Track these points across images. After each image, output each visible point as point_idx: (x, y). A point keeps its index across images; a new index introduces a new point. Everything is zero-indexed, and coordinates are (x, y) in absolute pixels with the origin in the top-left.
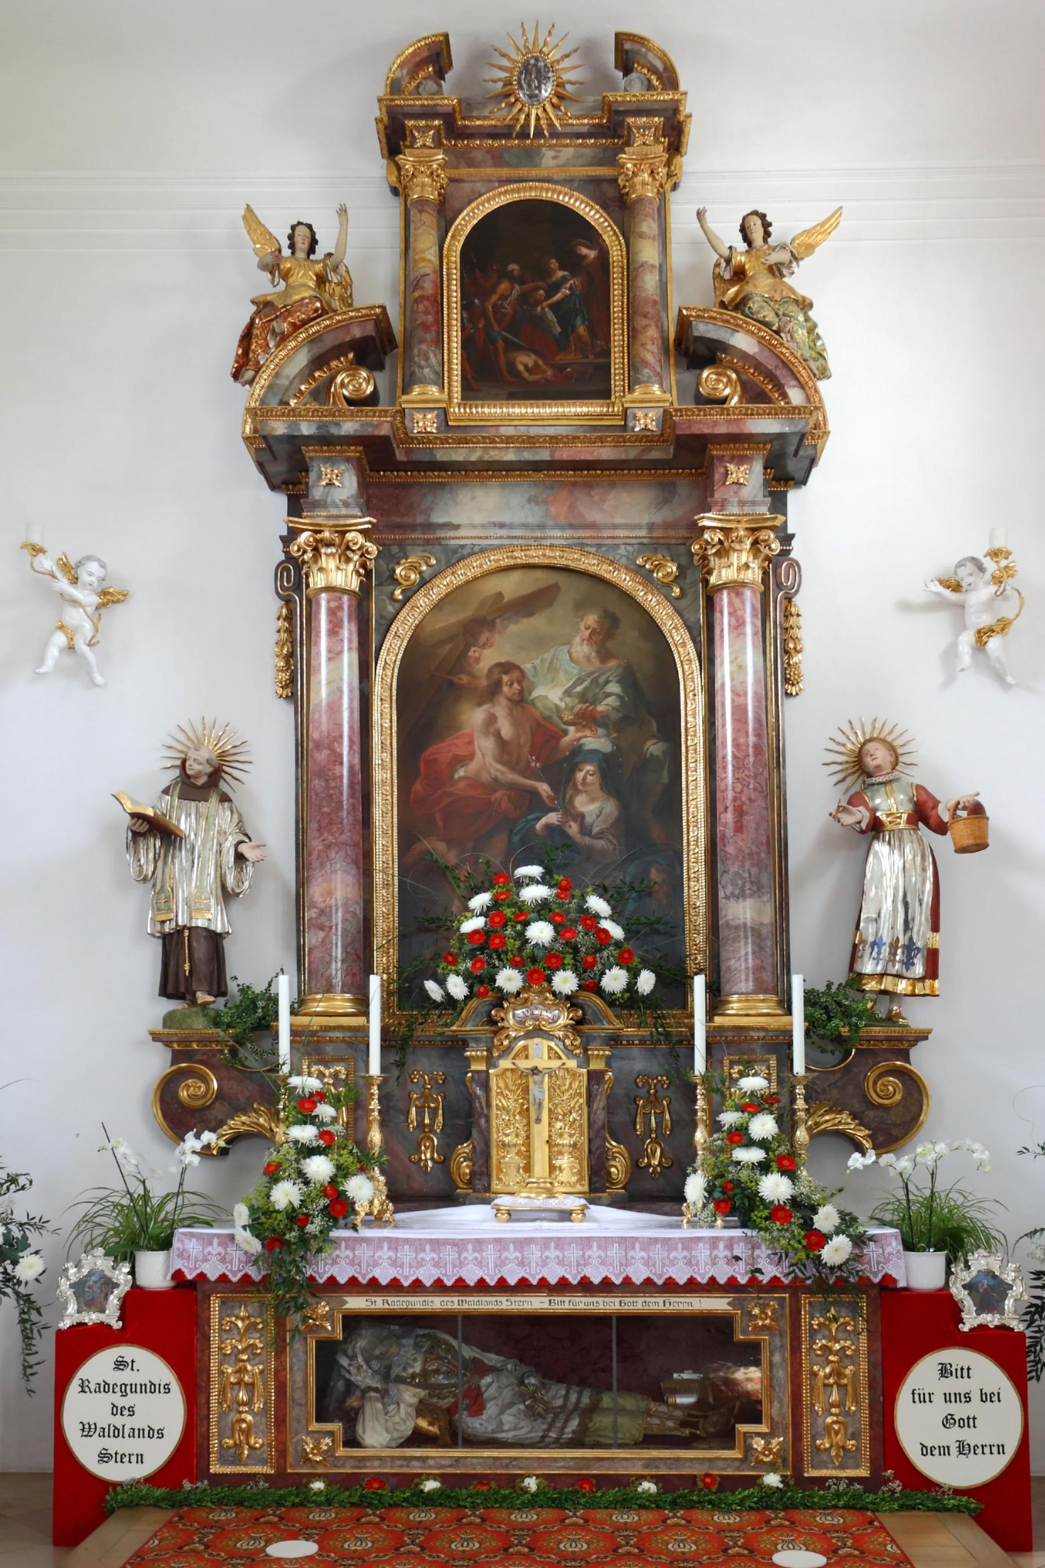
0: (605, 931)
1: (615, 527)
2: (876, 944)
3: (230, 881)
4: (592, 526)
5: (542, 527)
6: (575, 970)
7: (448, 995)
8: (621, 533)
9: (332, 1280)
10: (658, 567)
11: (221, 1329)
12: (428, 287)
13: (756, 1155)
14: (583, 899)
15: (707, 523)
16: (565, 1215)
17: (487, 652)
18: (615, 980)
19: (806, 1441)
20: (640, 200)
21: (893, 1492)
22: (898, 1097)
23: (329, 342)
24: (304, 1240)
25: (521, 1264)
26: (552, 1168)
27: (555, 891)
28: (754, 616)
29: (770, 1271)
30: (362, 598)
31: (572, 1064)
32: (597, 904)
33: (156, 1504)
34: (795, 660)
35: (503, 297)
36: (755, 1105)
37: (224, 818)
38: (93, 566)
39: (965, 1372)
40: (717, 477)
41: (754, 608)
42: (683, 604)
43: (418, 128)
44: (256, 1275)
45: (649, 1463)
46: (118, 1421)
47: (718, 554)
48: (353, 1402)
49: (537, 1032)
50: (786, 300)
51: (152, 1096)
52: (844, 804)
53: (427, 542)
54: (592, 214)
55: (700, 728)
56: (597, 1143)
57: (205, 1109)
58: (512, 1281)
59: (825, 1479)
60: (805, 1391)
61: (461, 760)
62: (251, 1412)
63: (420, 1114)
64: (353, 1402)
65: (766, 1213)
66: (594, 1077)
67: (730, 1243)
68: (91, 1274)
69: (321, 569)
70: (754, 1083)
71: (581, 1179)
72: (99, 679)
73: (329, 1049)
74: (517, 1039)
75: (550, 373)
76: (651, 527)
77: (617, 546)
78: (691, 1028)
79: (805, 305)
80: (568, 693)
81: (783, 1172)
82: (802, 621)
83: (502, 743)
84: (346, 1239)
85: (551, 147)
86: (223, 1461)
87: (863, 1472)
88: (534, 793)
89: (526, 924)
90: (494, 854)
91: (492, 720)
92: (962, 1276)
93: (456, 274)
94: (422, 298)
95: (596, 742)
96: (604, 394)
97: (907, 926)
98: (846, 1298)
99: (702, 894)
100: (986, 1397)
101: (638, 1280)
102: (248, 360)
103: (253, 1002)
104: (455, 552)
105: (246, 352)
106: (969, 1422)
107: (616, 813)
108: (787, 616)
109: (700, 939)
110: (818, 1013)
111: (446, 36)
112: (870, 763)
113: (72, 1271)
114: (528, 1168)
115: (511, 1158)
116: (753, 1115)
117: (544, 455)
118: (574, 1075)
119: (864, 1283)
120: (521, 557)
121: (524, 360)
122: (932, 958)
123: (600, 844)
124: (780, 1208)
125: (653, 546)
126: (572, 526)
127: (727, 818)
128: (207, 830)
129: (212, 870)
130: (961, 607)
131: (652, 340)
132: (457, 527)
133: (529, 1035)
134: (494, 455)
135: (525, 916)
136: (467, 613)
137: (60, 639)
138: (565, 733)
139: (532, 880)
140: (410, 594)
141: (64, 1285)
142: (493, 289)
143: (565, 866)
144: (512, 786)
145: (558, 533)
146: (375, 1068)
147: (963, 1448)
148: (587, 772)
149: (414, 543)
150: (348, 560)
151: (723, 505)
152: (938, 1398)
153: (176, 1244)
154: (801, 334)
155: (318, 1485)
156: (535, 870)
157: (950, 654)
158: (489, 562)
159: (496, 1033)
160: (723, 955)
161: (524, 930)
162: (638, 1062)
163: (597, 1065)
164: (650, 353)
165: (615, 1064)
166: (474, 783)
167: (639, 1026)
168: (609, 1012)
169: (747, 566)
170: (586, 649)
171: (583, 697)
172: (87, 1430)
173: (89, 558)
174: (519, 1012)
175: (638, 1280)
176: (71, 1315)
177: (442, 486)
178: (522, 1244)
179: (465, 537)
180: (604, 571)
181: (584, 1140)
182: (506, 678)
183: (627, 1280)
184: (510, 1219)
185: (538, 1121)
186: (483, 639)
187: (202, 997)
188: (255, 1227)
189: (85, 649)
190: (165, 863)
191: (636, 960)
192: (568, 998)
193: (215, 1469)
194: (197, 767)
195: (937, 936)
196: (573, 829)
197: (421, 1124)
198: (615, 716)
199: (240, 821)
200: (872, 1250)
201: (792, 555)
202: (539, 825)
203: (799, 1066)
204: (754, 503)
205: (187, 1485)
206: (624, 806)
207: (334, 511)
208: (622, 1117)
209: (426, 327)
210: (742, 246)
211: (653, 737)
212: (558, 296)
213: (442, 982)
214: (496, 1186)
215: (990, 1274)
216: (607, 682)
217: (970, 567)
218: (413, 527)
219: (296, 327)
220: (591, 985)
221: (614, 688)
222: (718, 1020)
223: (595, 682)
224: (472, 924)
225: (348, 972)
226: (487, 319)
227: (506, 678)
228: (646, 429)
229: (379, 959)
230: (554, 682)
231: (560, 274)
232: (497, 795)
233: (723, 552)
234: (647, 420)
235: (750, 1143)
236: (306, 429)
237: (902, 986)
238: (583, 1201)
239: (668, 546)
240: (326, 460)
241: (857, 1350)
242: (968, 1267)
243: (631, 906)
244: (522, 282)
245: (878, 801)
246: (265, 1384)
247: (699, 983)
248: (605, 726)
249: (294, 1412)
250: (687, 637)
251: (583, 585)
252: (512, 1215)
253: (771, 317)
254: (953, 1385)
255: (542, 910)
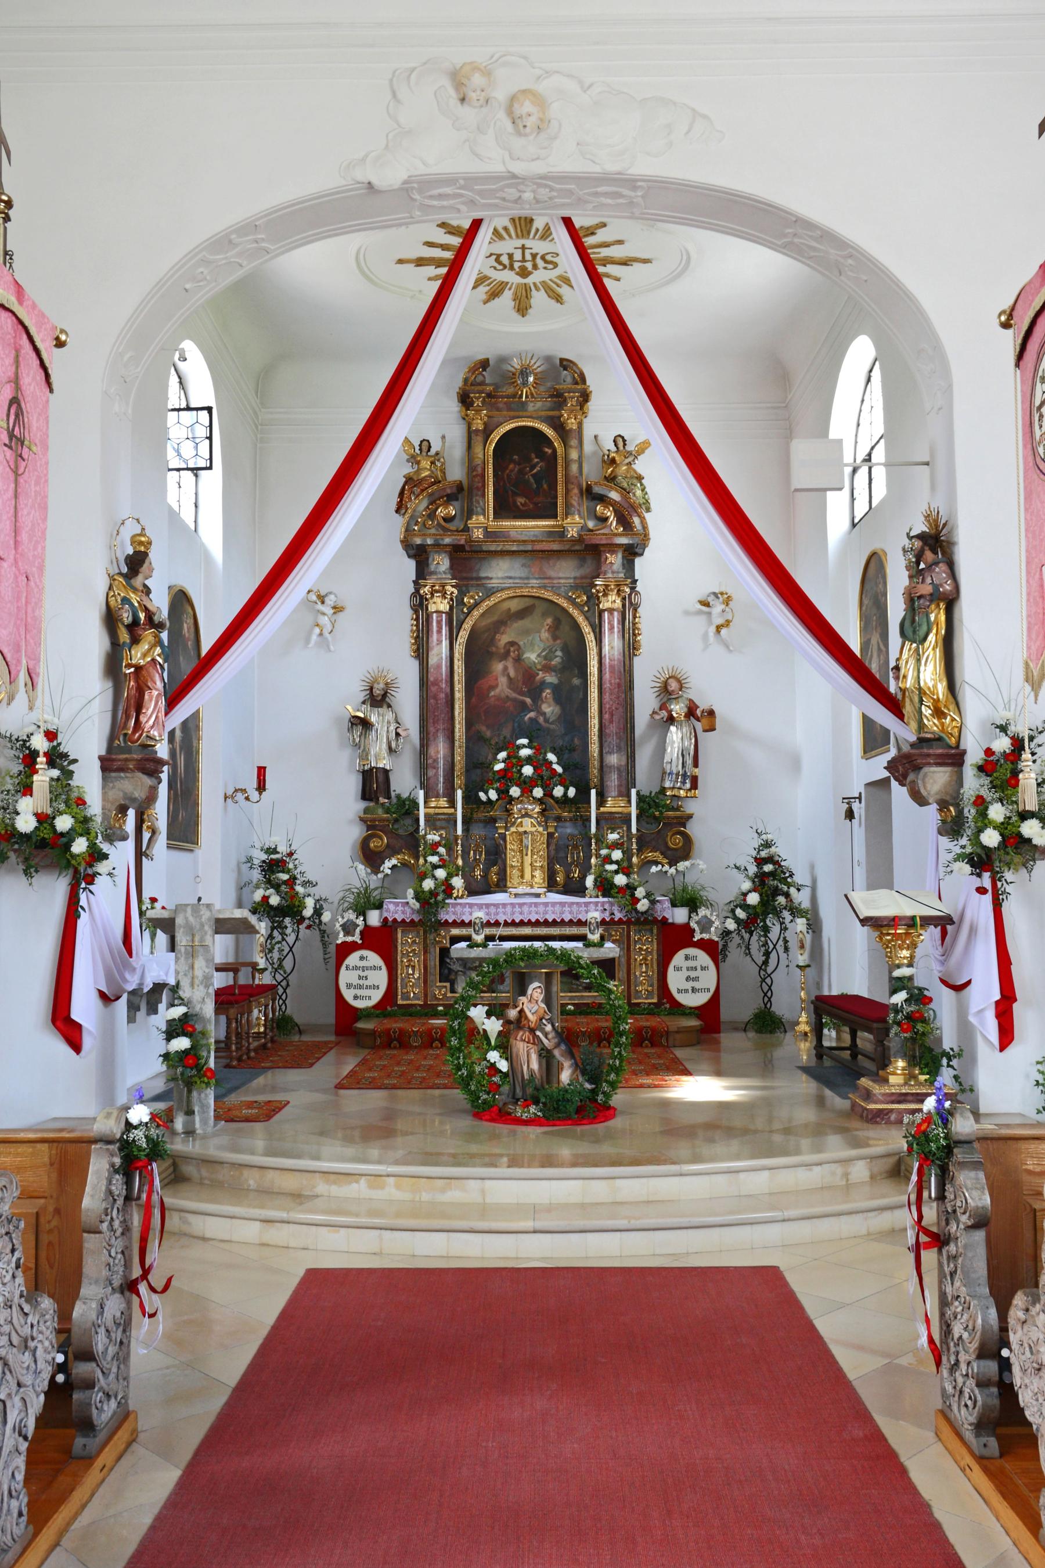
0: (555, 770)
1: (560, 578)
2: (671, 773)
3: (393, 745)
4: (549, 578)
5: (528, 578)
6: (542, 787)
7: (489, 799)
8: (562, 581)
9: (446, 920)
10: (579, 597)
11: (402, 943)
12: (479, 470)
13: (614, 867)
14: (545, 754)
15: (597, 583)
16: (538, 895)
17: (504, 636)
18: (558, 792)
19: (632, 988)
20: (571, 430)
21: (666, 1008)
22: (681, 844)
23: (437, 496)
24: (436, 902)
25: (521, 913)
26: (533, 876)
27: (533, 751)
28: (618, 623)
29: (618, 916)
30: (449, 614)
31: (541, 829)
32: (551, 757)
33: (377, 1016)
34: (638, 638)
35: (511, 471)
36: (614, 846)
37: (389, 716)
38: (332, 597)
39: (695, 958)
40: (603, 560)
41: (618, 620)
42: (588, 614)
43: (475, 397)
44: (416, 919)
45: (571, 998)
46: (361, 982)
47: (604, 595)
48: (452, 977)
49: (527, 815)
50: (632, 477)
51: (358, 847)
52: (657, 710)
53: (478, 585)
54: (549, 432)
55: (596, 673)
56: (551, 865)
57: (381, 852)
58: (517, 921)
59: (640, 1003)
60: (632, 966)
61: (493, 687)
62: (414, 978)
63: (475, 854)
64: (452, 977)
65: (616, 890)
66: (550, 835)
67: (603, 904)
68: (348, 921)
69: (434, 603)
70: (613, 837)
71: (544, 882)
72: (332, 647)
73: (438, 823)
74: (518, 818)
75: (531, 506)
76: (575, 578)
77: (560, 587)
78: (463, 808)
79: (640, 478)
80: (539, 656)
81: (624, 874)
82: (641, 620)
83: (510, 678)
84: (452, 904)
85: (532, 402)
86: (402, 999)
87: (655, 1001)
88: (524, 703)
89: (522, 766)
90: (506, 732)
91: (506, 668)
92: (695, 918)
93: (491, 461)
94: (477, 475)
95: (551, 679)
96: (554, 516)
97: (683, 766)
98: (648, 927)
99: (597, 750)
100: (703, 968)
101: (567, 920)
102: (402, 504)
103: (404, 801)
104: (490, 590)
105: (401, 500)
106: (696, 979)
107: (559, 712)
108: (635, 617)
109: (596, 771)
110: (645, 806)
111: (488, 359)
112: (670, 689)
113: (340, 919)
114: (522, 877)
115: (516, 872)
116: (613, 850)
117: (529, 548)
118: (542, 834)
119: (655, 921)
120: (519, 592)
121: (520, 500)
122: (694, 781)
123: (552, 727)
124: (622, 888)
125: (575, 588)
126: (540, 578)
127: (606, 716)
128: (383, 721)
129: (385, 740)
130: (710, 614)
131: (575, 494)
132: (491, 579)
133: (523, 816)
134: (508, 548)
135: (522, 762)
136: (495, 618)
137: (317, 631)
138: (538, 674)
139: (524, 746)
140: (471, 609)
141: (338, 925)
142: (507, 468)
143: (537, 737)
144: (515, 700)
145: (535, 581)
146: (459, 832)
147: (694, 990)
148: (547, 693)
149: (472, 586)
150: (445, 598)
151: (605, 573)
152: (684, 969)
153: (385, 906)
154: (639, 493)
155: (441, 1008)
156: (524, 741)
157: (705, 636)
158: (504, 595)
159: (509, 816)
160: (605, 779)
161: (521, 769)
162: (569, 829)
163: (551, 830)
164: (574, 501)
165: (559, 830)
166: (498, 698)
167: (569, 812)
168: (556, 805)
169: (615, 601)
170: (547, 635)
171: (545, 658)
172: (349, 986)
173: (330, 593)
174: (519, 806)
175: (567, 920)
176: (341, 938)
177: (484, 558)
178: (521, 905)
179: (494, 583)
180: (555, 599)
181: (546, 863)
182: (512, 649)
183: (563, 920)
184: (515, 897)
185: (527, 855)
186: (502, 630)
187: (382, 800)
188: (417, 897)
189: (328, 635)
190: (365, 737)
191: (568, 782)
192: (539, 799)
193: (400, 1002)
194: (378, 692)
195: (696, 770)
196: (541, 719)
197: (475, 859)
198: (559, 667)
199: (396, 717)
200: (658, 906)
201: (637, 589)
202: (526, 718)
203: (634, 830)
204: (618, 572)
205: (389, 1008)
206: (563, 709)
207: (439, 576)
208: (562, 854)
209: (478, 489)
210: (614, 449)
211: (575, 676)
212: (535, 471)
213: (486, 793)
214: (509, 884)
215: (706, 917)
216: (556, 650)
217: (712, 597)
218: (472, 579)
219: (423, 491)
220: (548, 794)
221: (559, 653)
222: (602, 809)
223: (550, 651)
224: (499, 766)
225: (445, 788)
226: (504, 481)
227: (512, 649)
228: (573, 536)
229: (457, 782)
230: (533, 651)
231: (536, 460)
232: (508, 704)
233: (605, 595)
234: (572, 532)
235: (612, 862)
236: (429, 541)
237: (682, 793)
238: (545, 890)
239: (583, 587)
240: (436, 552)
241: (652, 949)
242: (697, 914)
243: (566, 756)
244: (519, 464)
245: (672, 707)
246: (419, 965)
247: (593, 792)
248: (555, 671)
249: (430, 978)
250: (590, 630)
251: (545, 605)
252: (516, 895)
253: (625, 485)
254: (691, 964)
255: (529, 760)
